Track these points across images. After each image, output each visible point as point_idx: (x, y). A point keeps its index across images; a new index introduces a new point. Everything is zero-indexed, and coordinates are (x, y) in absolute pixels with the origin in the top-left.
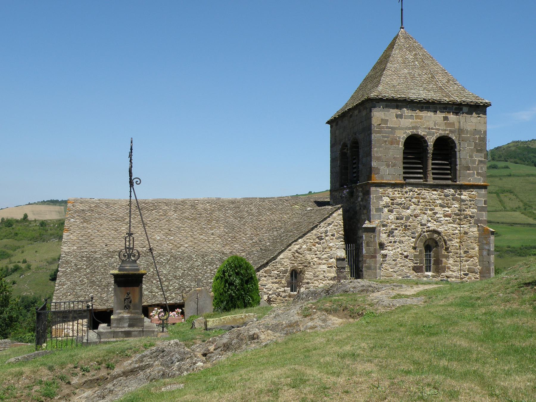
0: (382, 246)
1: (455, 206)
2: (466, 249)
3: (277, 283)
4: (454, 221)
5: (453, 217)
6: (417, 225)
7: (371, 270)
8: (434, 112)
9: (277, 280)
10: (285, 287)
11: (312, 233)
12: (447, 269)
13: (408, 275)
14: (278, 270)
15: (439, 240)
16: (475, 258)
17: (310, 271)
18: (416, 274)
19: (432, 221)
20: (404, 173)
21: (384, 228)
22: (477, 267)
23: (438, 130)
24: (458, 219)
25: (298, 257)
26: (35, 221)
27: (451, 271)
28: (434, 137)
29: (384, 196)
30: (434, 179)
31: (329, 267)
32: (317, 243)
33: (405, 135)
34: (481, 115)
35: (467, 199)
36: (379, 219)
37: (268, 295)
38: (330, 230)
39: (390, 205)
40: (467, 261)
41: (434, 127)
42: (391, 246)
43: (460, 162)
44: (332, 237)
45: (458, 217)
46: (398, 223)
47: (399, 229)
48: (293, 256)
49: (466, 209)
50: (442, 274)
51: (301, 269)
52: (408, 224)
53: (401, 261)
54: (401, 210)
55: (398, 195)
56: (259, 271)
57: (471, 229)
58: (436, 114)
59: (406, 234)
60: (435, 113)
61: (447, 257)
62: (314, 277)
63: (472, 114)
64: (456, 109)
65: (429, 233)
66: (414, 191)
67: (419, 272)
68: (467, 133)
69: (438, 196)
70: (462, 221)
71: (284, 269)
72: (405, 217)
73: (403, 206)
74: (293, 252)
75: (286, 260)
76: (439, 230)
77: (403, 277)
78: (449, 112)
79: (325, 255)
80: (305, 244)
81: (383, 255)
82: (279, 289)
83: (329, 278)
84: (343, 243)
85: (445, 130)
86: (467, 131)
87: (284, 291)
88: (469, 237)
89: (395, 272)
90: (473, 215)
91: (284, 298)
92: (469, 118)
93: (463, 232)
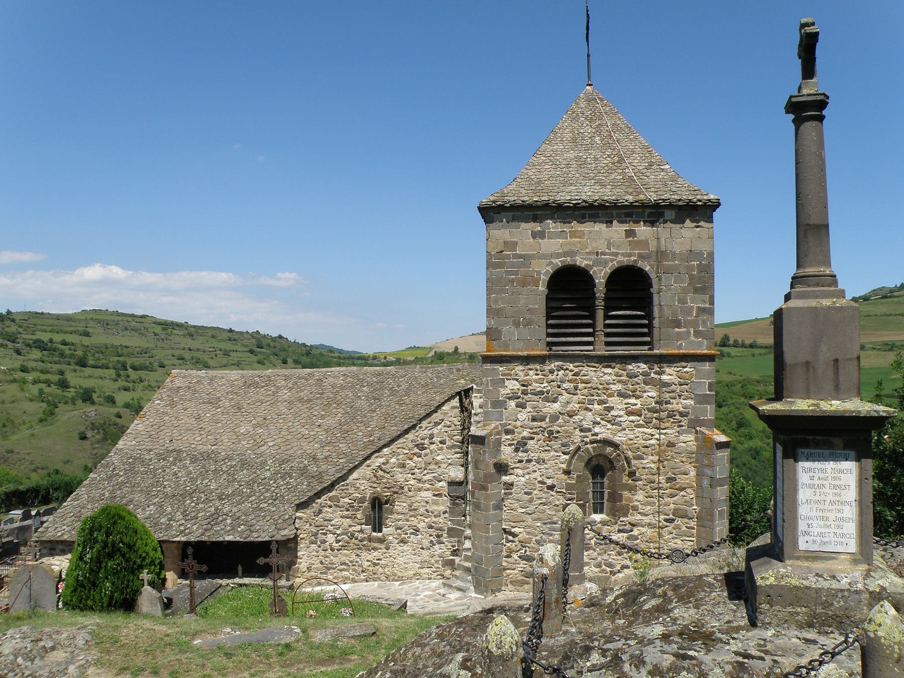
0: (502, 468)
2: (670, 474)
3: (350, 518)
4: (646, 423)
5: (646, 414)
6: (572, 431)
8: (607, 222)
9: (348, 513)
10: (363, 524)
11: (406, 439)
12: (631, 511)
13: (555, 519)
15: (615, 457)
16: (689, 490)
19: (603, 423)
20: (549, 335)
21: (508, 437)
22: (691, 508)
23: (616, 254)
24: (656, 418)
25: (383, 477)
26: (465, 353)
29: (508, 379)
30: (608, 344)
31: (435, 495)
32: (415, 454)
33: (549, 268)
34: (702, 223)
36: (499, 421)
37: (336, 536)
38: (438, 434)
39: (519, 394)
40: (672, 496)
41: (607, 251)
42: (523, 469)
44: (441, 445)
45: (655, 415)
46: (536, 428)
49: (671, 400)
50: (621, 520)
51: (389, 497)
52: (555, 428)
54: (541, 404)
55: (535, 377)
56: (319, 498)
57: (681, 438)
58: (612, 227)
61: (632, 489)
63: (683, 222)
64: (650, 215)
65: (595, 445)
66: (567, 369)
68: (674, 259)
69: (615, 378)
70: (663, 422)
71: (360, 496)
72: (548, 416)
73: (546, 396)
74: (374, 469)
75: (363, 482)
76: (617, 439)
77: (545, 524)
79: (428, 476)
80: (395, 457)
81: (505, 483)
83: (436, 513)
85: (630, 255)
86: (674, 254)
87: (361, 531)
88: (677, 451)
89: (530, 514)
91: (360, 541)
93: (666, 442)
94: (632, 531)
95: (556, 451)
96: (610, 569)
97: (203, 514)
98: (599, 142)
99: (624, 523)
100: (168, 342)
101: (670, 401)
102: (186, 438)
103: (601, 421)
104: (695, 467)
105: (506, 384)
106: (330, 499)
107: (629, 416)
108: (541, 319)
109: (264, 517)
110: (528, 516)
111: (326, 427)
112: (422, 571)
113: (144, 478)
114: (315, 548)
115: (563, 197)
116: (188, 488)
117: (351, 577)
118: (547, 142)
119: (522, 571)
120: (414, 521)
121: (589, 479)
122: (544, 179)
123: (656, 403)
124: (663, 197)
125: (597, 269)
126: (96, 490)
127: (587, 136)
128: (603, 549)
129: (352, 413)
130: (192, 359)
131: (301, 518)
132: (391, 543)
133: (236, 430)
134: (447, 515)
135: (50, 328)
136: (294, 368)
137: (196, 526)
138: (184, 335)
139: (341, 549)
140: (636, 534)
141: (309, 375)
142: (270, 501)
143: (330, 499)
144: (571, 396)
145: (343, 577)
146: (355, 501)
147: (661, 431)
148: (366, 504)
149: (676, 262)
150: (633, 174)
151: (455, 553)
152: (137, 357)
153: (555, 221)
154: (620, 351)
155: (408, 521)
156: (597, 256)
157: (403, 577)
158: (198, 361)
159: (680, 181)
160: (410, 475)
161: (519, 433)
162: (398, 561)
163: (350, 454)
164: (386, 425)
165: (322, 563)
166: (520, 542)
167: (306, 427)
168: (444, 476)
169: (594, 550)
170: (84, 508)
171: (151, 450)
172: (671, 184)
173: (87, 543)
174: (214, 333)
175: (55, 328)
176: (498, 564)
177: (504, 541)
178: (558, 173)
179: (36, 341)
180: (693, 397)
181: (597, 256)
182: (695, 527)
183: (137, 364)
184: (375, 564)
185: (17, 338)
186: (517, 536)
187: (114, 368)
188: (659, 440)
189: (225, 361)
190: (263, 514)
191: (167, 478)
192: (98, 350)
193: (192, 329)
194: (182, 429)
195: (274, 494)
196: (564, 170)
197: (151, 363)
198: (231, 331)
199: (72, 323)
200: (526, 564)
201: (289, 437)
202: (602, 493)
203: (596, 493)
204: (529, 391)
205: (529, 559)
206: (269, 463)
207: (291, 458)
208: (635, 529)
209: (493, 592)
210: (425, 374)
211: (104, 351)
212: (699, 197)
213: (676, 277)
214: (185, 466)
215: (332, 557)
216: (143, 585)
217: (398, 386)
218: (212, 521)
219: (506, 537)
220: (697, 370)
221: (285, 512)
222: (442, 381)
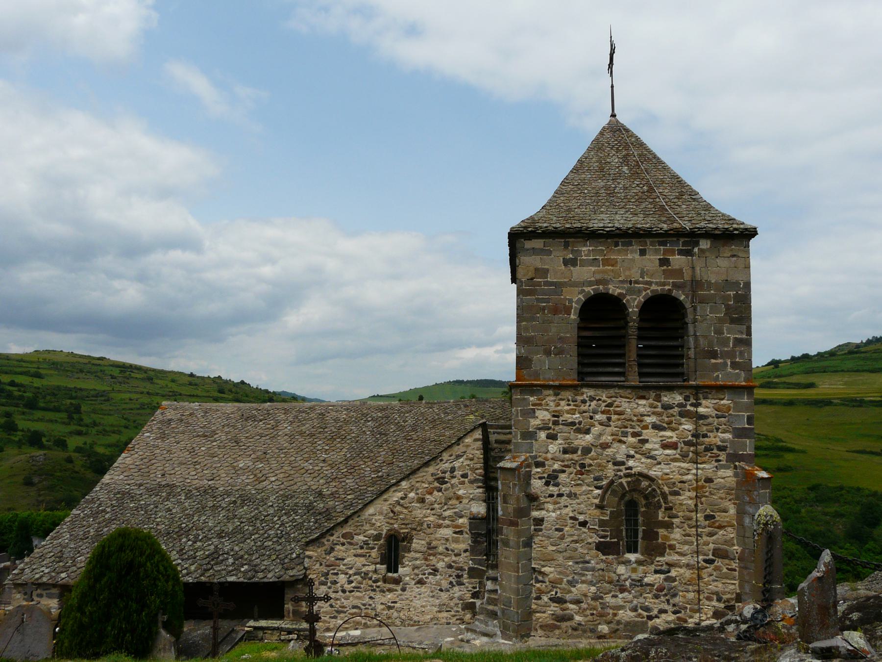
1: (686, 427)
2: (708, 512)
3: (364, 556)
5: (682, 448)
6: (605, 464)
7: (509, 547)
9: (362, 551)
13: (587, 558)
14: (364, 534)
16: (729, 529)
17: (421, 538)
18: (604, 558)
19: (637, 456)
21: (539, 470)
23: (650, 283)
27: (676, 553)
28: (640, 297)
29: (538, 409)
31: (455, 533)
32: (436, 488)
33: (581, 296)
35: (711, 413)
36: (529, 453)
38: (459, 467)
39: (550, 425)
40: (711, 535)
41: (641, 279)
43: (694, 343)
45: (692, 449)
48: (392, 511)
52: (587, 461)
56: (332, 535)
59: (583, 481)
61: (669, 526)
62: (429, 548)
65: (629, 479)
66: (600, 400)
68: (709, 289)
69: (649, 409)
71: (375, 533)
72: (580, 449)
76: (652, 473)
82: (367, 567)
83: (456, 551)
84: (481, 490)
85: (664, 284)
86: (709, 283)
88: (715, 487)
90: (725, 444)
91: (375, 582)
92: (713, 259)
95: (588, 486)
97: (202, 552)
98: (627, 172)
101: (707, 434)
102: (179, 472)
103: (635, 455)
104: (734, 504)
105: (536, 415)
106: (344, 536)
107: (664, 449)
109: (270, 556)
110: (559, 555)
111: (331, 462)
112: (440, 615)
114: (325, 590)
116: (184, 525)
117: (363, 621)
119: (553, 614)
121: (623, 516)
122: (573, 207)
123: (693, 436)
125: (631, 298)
126: (80, 527)
128: (638, 591)
129: (357, 448)
131: (310, 557)
133: (235, 464)
134: (468, 554)
138: (143, 379)
139: (352, 591)
141: (310, 408)
142: (275, 540)
143: (344, 536)
144: (604, 427)
146: (369, 538)
148: (382, 541)
149: (712, 292)
150: (664, 204)
151: (475, 595)
152: (92, 400)
154: (652, 381)
156: (631, 284)
157: (419, 622)
160: (429, 511)
161: (550, 466)
162: (414, 604)
163: (358, 490)
164: (394, 460)
166: (550, 582)
167: (310, 462)
168: (465, 511)
169: (630, 592)
170: (65, 547)
171: (141, 485)
176: (527, 607)
177: (533, 582)
178: (588, 201)
181: (631, 284)
182: (737, 569)
184: (390, 608)
186: (547, 575)
187: (66, 411)
190: (268, 553)
194: (175, 462)
195: (279, 532)
196: (593, 198)
198: (192, 375)
199: (23, 363)
200: (557, 607)
201: (292, 472)
202: (636, 531)
204: (561, 422)
207: (295, 494)
209: (522, 637)
210: (431, 410)
213: (711, 308)
214: (179, 502)
215: (343, 600)
217: (405, 421)
219: (536, 577)
220: (735, 403)
221: (292, 551)
222: (449, 417)
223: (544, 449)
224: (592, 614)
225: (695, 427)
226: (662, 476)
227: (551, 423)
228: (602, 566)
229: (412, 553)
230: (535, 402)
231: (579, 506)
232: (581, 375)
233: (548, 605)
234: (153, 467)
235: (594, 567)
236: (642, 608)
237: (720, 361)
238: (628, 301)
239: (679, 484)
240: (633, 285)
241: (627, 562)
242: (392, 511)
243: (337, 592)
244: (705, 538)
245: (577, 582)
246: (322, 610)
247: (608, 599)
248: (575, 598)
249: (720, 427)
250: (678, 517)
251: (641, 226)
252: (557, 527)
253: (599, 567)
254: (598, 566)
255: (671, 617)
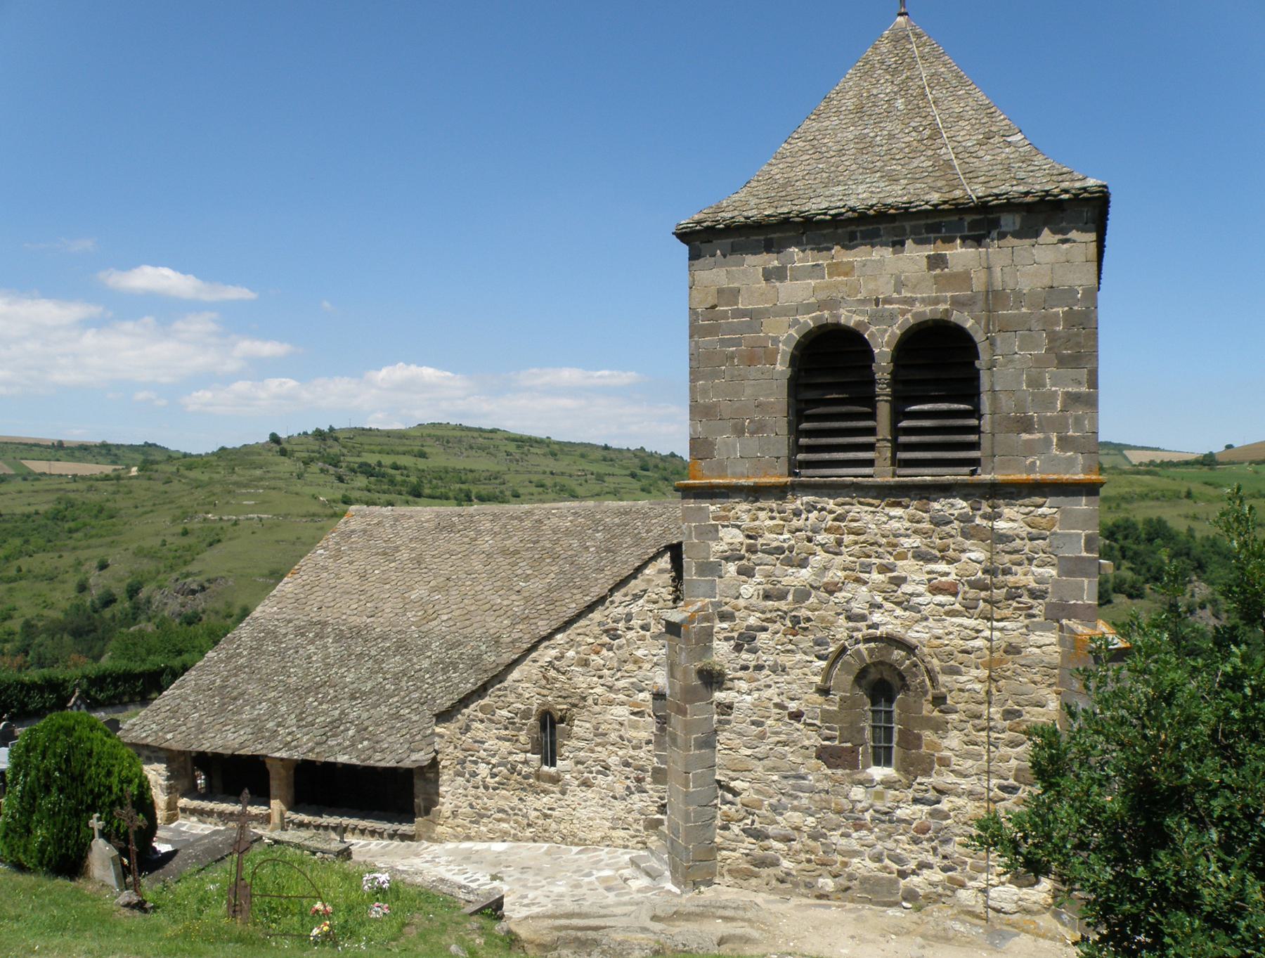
0: (712, 679)
1: (973, 555)
2: (1010, 704)
3: (509, 740)
4: (967, 608)
5: (965, 592)
6: (832, 619)
8: (894, 244)
9: (507, 732)
11: (591, 620)
12: (937, 767)
13: (803, 771)
15: (908, 668)
18: (829, 772)
19: (888, 605)
20: (976, 430)
21: (725, 625)
23: (910, 301)
24: (985, 601)
25: (556, 679)
27: (952, 771)
28: (894, 327)
29: (723, 526)
30: (898, 463)
31: (633, 714)
32: (603, 645)
33: (792, 332)
34: (1074, 235)
35: (1019, 531)
36: (710, 597)
38: (638, 613)
39: (743, 552)
41: (895, 295)
44: (642, 632)
45: (983, 594)
46: (771, 611)
47: (772, 627)
49: (1014, 568)
50: (919, 780)
52: (804, 613)
53: (779, 727)
56: (466, 707)
58: (903, 252)
60: (898, 247)
61: (940, 727)
63: (1037, 234)
64: (973, 226)
65: (873, 645)
66: (823, 509)
67: (837, 767)
69: (908, 525)
70: (998, 608)
71: (523, 707)
72: (792, 592)
73: (787, 557)
75: (528, 685)
76: (912, 636)
78: (949, 240)
81: (720, 704)
83: (634, 742)
85: (936, 301)
86: (1019, 297)
87: (526, 762)
88: (1023, 662)
90: (1043, 587)
93: (1004, 645)
94: (938, 802)
95: (805, 653)
96: (897, 867)
97: (323, 719)
99: (923, 787)
100: (525, 464)
101: (1010, 569)
102: (338, 605)
103: (884, 603)
104: (1058, 693)
105: (721, 535)
106: (482, 709)
107: (934, 595)
108: (779, 422)
109: (399, 729)
111: (527, 594)
112: (614, 834)
113: (268, 661)
115: (815, 206)
116: (318, 679)
117: (513, 832)
118: (813, 117)
119: (747, 855)
120: (602, 753)
123: (985, 571)
124: (996, 191)
127: (882, 99)
128: (885, 830)
130: (555, 486)
131: (441, 736)
132: (568, 784)
133: (406, 595)
134: (651, 747)
135: (380, 447)
136: (368, 504)
137: (308, 737)
138: (544, 455)
139: (498, 788)
140: (946, 809)
143: (482, 709)
144: (831, 556)
145: (500, 831)
146: (516, 714)
147: (995, 623)
148: (532, 720)
153: (803, 248)
154: (926, 476)
155: (592, 751)
156: (877, 305)
158: (563, 489)
159: (1038, 160)
160: (595, 679)
161: (744, 619)
162: (578, 815)
165: (471, 806)
166: (743, 805)
167: (499, 593)
169: (871, 831)
171: (290, 621)
172: (1020, 167)
173: (21, 769)
174: (583, 451)
175: (385, 447)
176: (706, 839)
177: (718, 801)
179: (362, 465)
180: (1056, 561)
181: (877, 305)
183: (484, 493)
184: (546, 816)
185: (339, 462)
188: (990, 640)
189: (597, 488)
191: (297, 662)
192: (435, 475)
193: (556, 447)
196: (833, 160)
197: (502, 492)
198: (606, 448)
202: (889, 731)
203: (878, 730)
204: (759, 546)
205: (759, 835)
206: (433, 646)
208: (945, 799)
209: (696, 885)
211: (443, 475)
212: (1065, 185)
216: (93, 837)
218: (331, 730)
219: (722, 796)
220: (1064, 512)
223: (733, 592)
224: (809, 861)
225: (989, 554)
226: (929, 641)
227: (744, 548)
228: (826, 785)
229: (574, 740)
230: (718, 514)
231: (790, 686)
232: (794, 467)
233: (740, 838)
234: (313, 597)
235: (814, 786)
236: (889, 857)
237: (1037, 436)
238: (872, 334)
239: (960, 655)
240: (880, 306)
241: (867, 783)
242: (544, 677)
243: (478, 788)
244: (1004, 750)
245: (785, 809)
246: (460, 810)
247: (835, 837)
248: (783, 832)
249: (1036, 556)
250: (957, 712)
251: (894, 200)
252: (754, 718)
253: (821, 787)
254: (820, 786)
255: (937, 876)
